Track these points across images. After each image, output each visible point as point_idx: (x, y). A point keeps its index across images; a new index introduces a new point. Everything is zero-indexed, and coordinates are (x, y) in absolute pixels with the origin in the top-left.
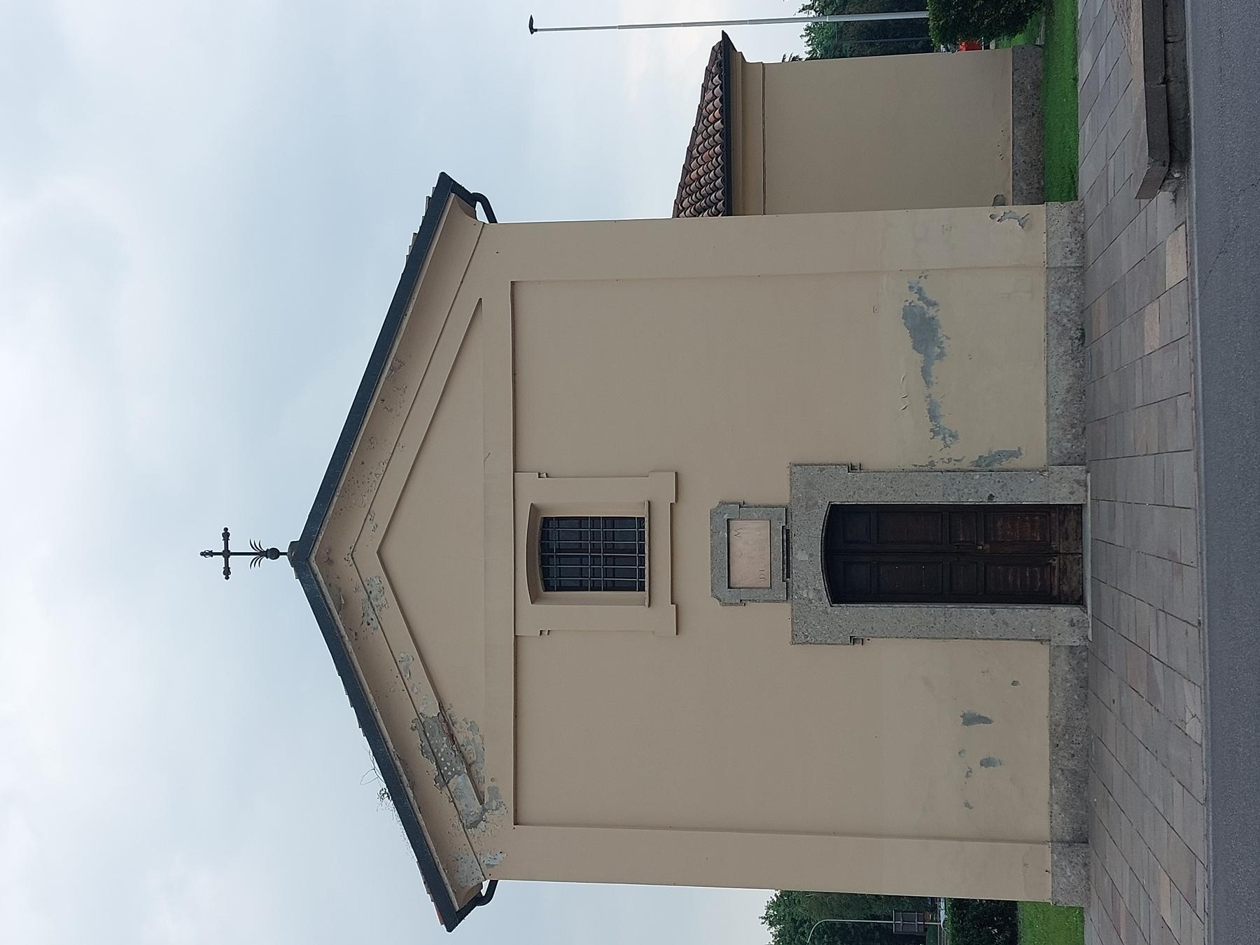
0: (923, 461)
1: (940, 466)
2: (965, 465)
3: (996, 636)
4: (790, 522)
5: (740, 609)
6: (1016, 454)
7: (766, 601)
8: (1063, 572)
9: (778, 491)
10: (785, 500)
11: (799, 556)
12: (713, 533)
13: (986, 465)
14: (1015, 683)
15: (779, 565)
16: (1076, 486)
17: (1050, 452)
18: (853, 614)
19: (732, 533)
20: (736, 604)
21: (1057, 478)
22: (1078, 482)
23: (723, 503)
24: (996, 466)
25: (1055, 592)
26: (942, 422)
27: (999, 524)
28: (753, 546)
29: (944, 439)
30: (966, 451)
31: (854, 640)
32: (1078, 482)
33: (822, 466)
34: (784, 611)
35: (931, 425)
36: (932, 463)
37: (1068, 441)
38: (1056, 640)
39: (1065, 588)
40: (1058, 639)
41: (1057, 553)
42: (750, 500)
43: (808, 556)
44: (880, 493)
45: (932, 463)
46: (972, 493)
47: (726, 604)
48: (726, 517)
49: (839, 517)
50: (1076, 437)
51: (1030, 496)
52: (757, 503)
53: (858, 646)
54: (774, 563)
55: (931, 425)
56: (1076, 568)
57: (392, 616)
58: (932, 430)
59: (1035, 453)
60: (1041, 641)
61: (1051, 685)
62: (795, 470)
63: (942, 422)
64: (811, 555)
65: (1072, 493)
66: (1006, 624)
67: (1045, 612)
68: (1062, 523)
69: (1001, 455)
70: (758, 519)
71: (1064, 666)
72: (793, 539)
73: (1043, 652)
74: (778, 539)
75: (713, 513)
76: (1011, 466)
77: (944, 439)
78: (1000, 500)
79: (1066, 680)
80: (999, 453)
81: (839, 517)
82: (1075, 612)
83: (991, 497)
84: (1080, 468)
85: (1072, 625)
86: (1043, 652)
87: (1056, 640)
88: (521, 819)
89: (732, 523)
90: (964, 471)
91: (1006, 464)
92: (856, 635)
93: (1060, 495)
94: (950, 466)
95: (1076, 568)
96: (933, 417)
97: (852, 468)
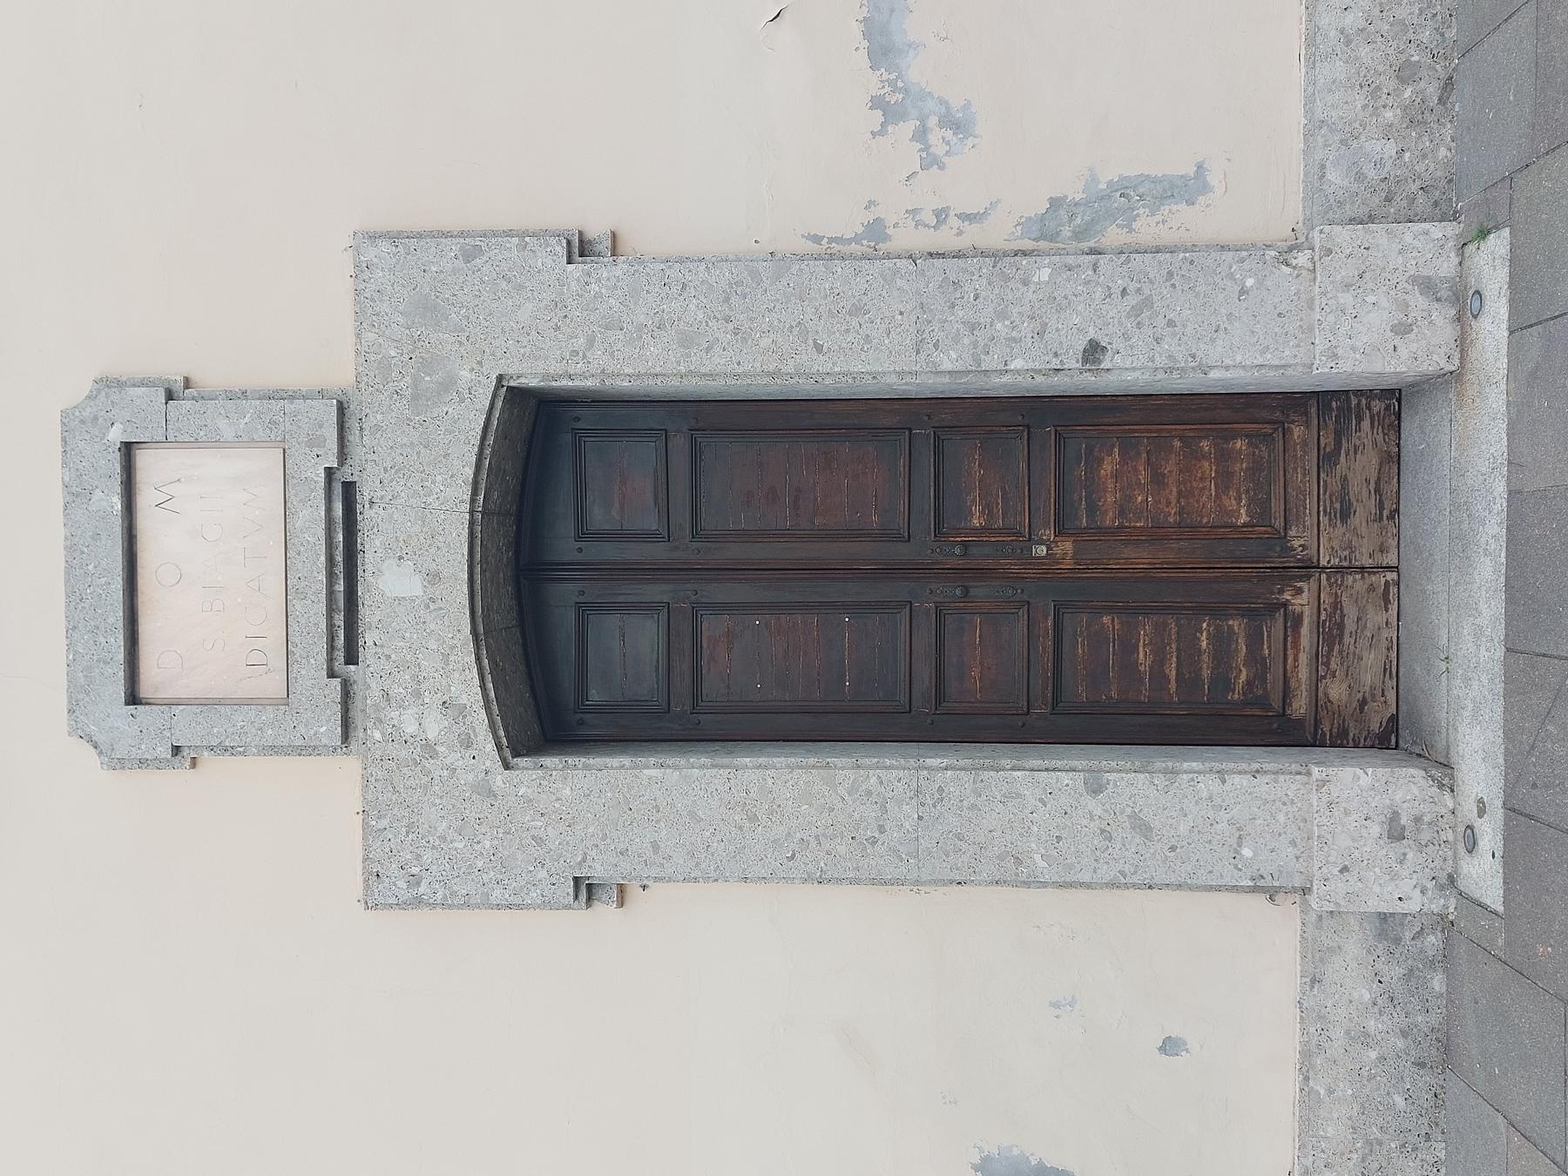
0: (844, 221)
1: (906, 238)
2: (998, 233)
3: (1107, 873)
4: (357, 452)
5: (178, 779)
6: (1187, 188)
7: (273, 750)
8: (1331, 632)
9: (316, 343)
10: (340, 372)
11: (389, 581)
12: (75, 495)
13: (1073, 231)
14: (1170, 1046)
15: (312, 612)
16: (1418, 301)
17: (1317, 175)
18: (592, 794)
19: (146, 498)
20: (158, 764)
21: (1348, 272)
22: (1427, 286)
23: (109, 384)
24: (1113, 236)
25: (1300, 706)
26: (917, 71)
27: (1107, 467)
28: (225, 540)
29: (921, 134)
30: (1003, 183)
31: (586, 890)
32: (1427, 286)
33: (472, 244)
34: (321, 799)
35: (873, 82)
36: (876, 230)
37: (1387, 133)
38: (1330, 892)
39: (1336, 691)
40: (1339, 887)
41: (1309, 567)
42: (210, 375)
43: (425, 581)
44: (686, 341)
45: (876, 230)
46: (1017, 347)
47: (120, 764)
48: (116, 435)
49: (542, 443)
50: (1415, 118)
51: (1239, 348)
52: (237, 382)
53: (604, 911)
54: (297, 606)
55: (873, 82)
56: (1375, 618)
57: (962, 763)
58: (877, 103)
59: (1262, 189)
60: (1272, 894)
61: (1306, 1055)
62: (370, 254)
63: (917, 71)
64: (433, 578)
65: (1402, 329)
66: (1143, 829)
67: (1289, 786)
68: (1327, 459)
69: (1130, 195)
70: (239, 442)
71: (1354, 980)
72: (368, 517)
73: (1275, 934)
74: (312, 516)
75: (73, 425)
76: (1167, 237)
77: (921, 134)
78: (1133, 368)
79: (1365, 1038)
80: (1123, 188)
81: (542, 443)
82: (1395, 785)
83: (1094, 351)
84: (1437, 230)
85: (1395, 833)
86: (1275, 934)
87: (1330, 892)
88: (145, 691)
89: (143, 458)
90: (996, 255)
91: (1148, 229)
92: (597, 871)
93: (1352, 344)
94: (945, 239)
95: (1375, 618)
96: (882, 48)
97: (581, 249)
